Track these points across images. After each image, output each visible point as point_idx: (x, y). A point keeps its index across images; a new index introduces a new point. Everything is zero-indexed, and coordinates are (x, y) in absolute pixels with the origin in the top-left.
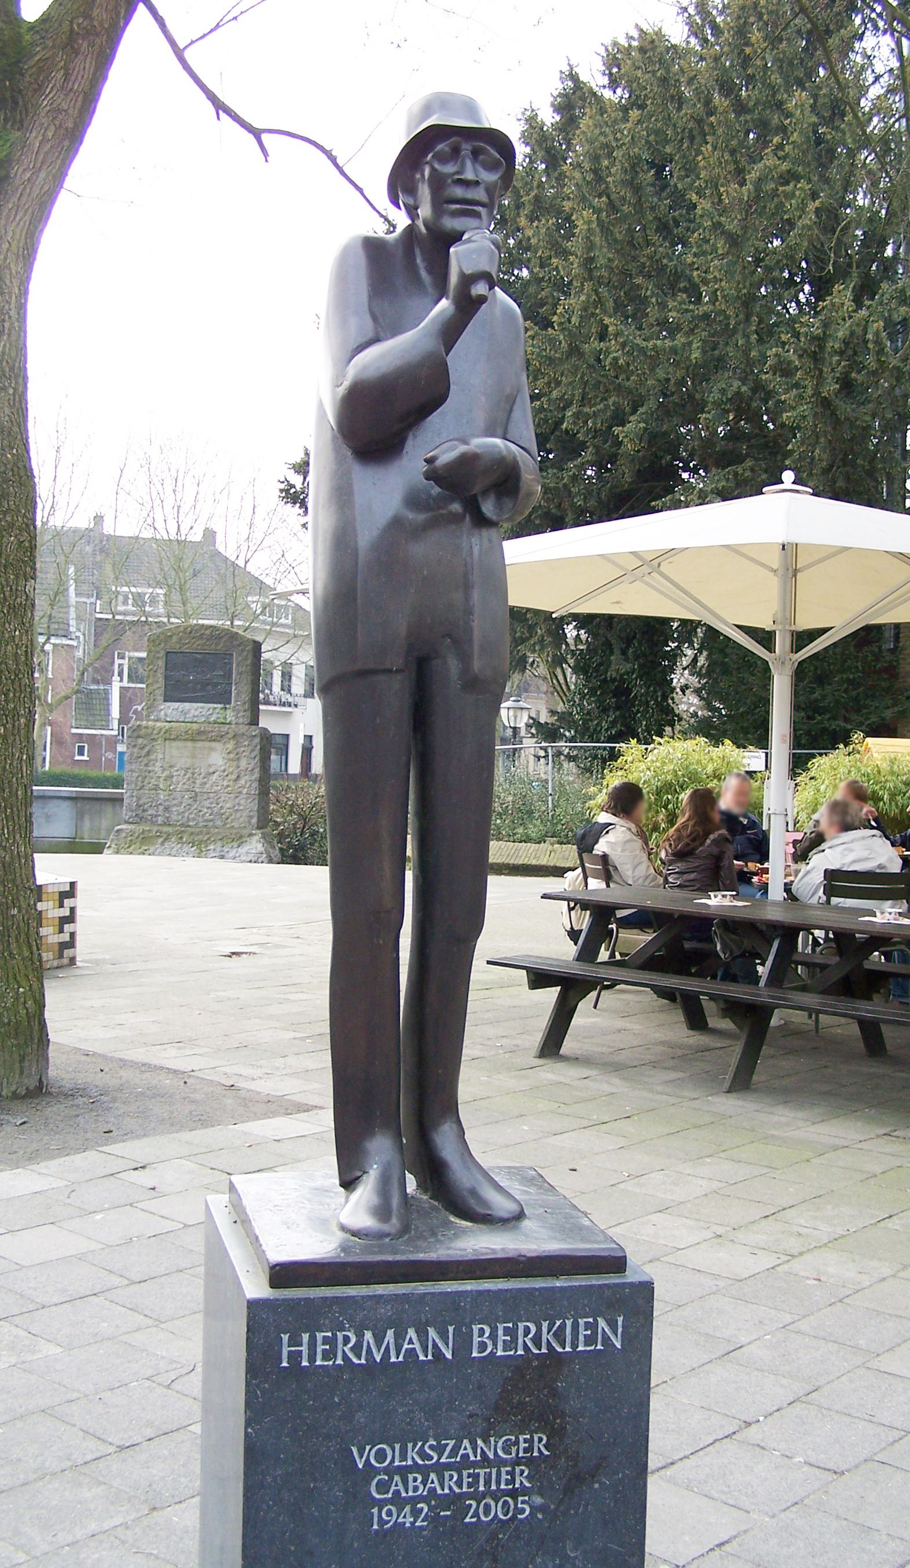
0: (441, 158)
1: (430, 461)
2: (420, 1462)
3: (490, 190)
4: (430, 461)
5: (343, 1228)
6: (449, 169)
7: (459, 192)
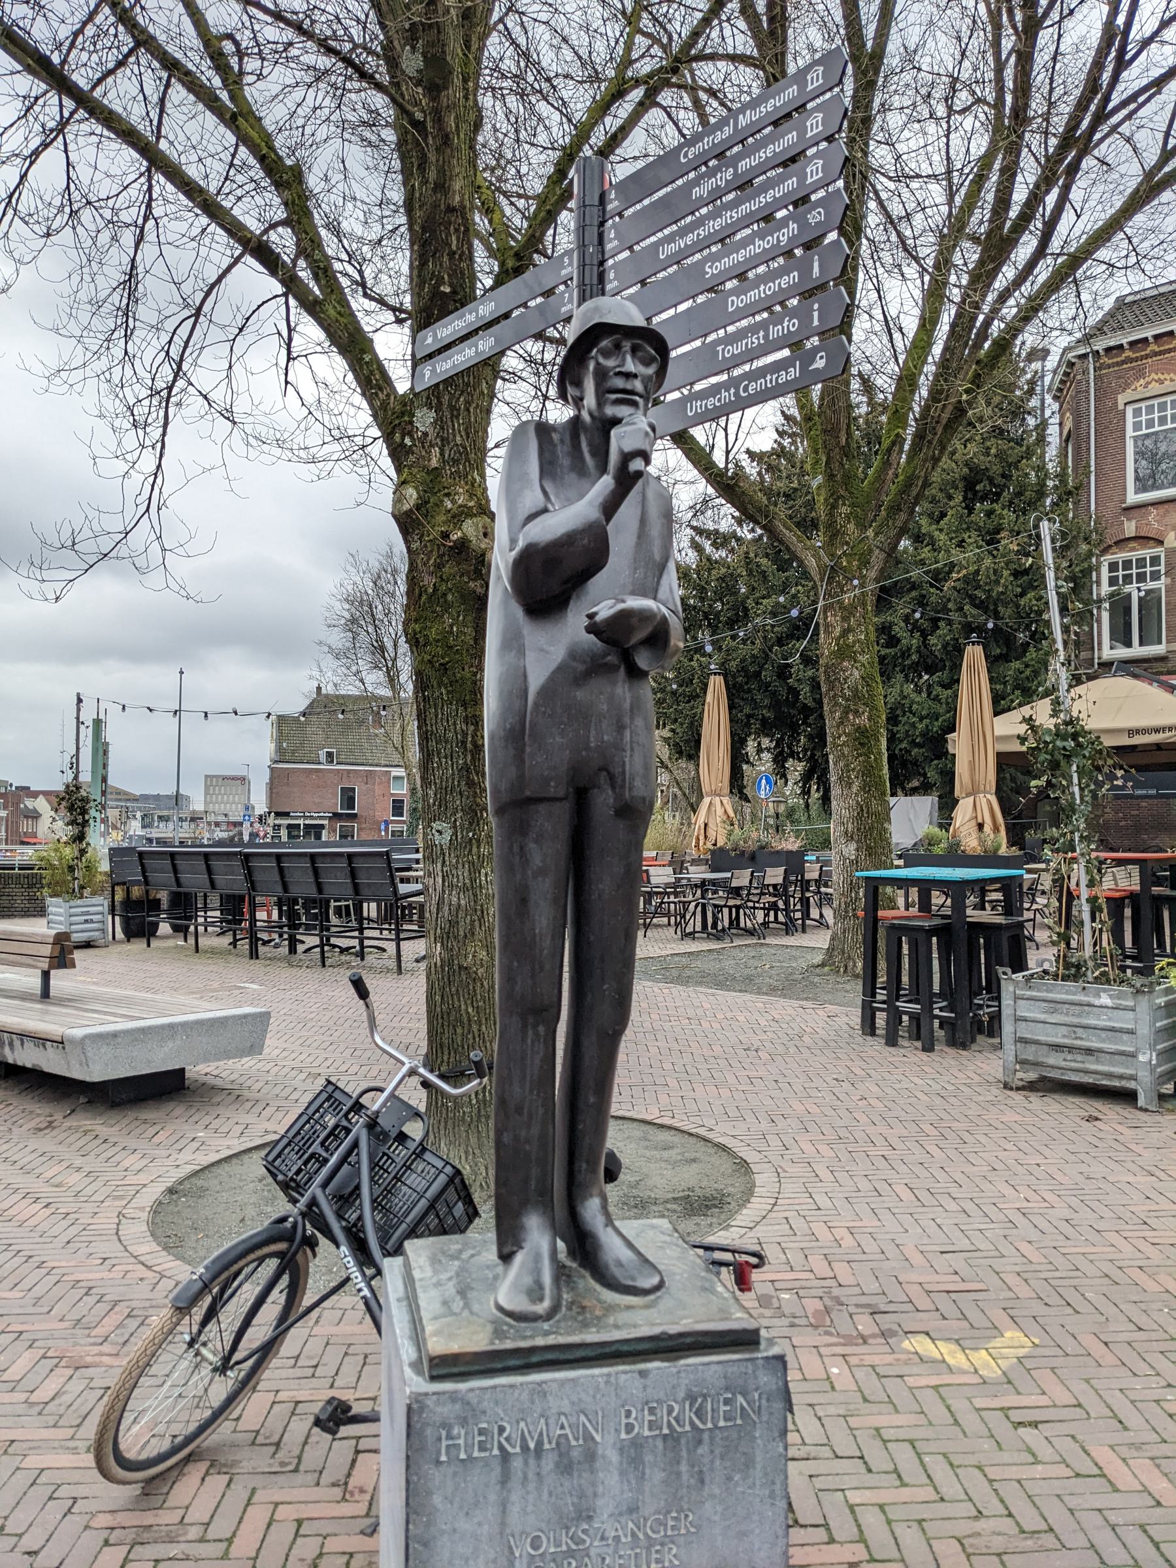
0: (606, 354)
1: (591, 616)
2: (574, 1547)
3: (646, 381)
4: (591, 616)
5: (500, 1308)
6: (610, 363)
7: (620, 383)
